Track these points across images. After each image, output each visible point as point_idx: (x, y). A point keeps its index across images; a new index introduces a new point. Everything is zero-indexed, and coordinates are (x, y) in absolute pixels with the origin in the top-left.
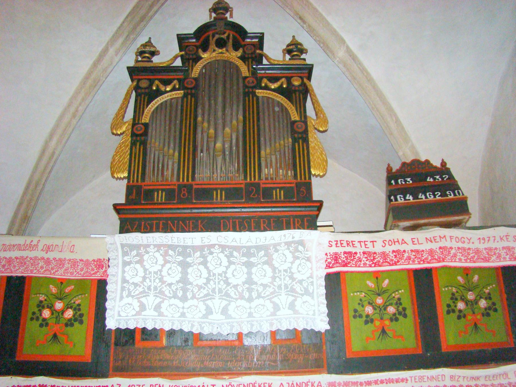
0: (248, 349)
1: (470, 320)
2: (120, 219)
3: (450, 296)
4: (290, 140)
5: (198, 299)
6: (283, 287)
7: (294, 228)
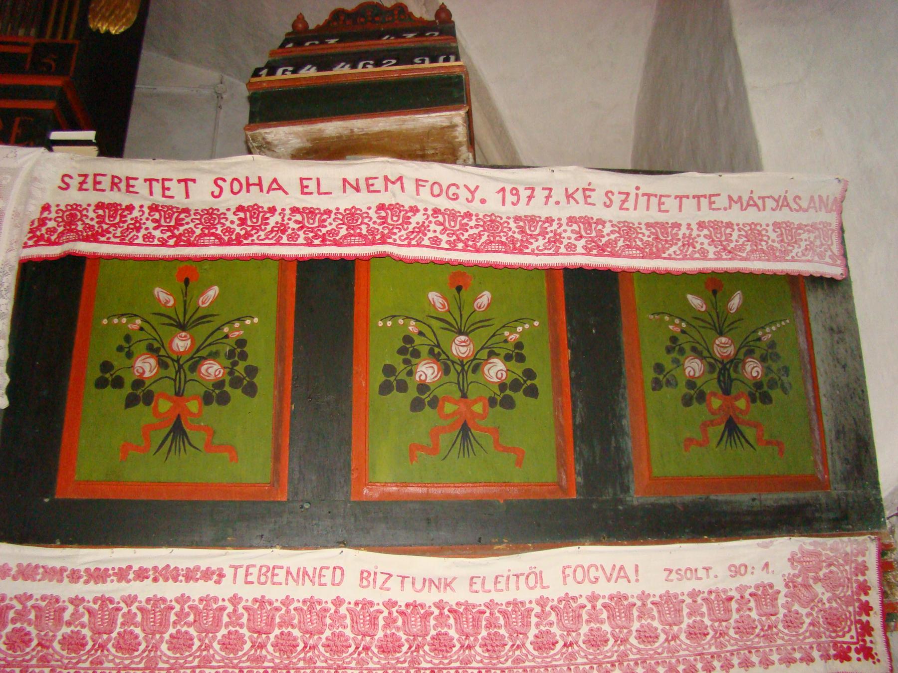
1: (448, 416)
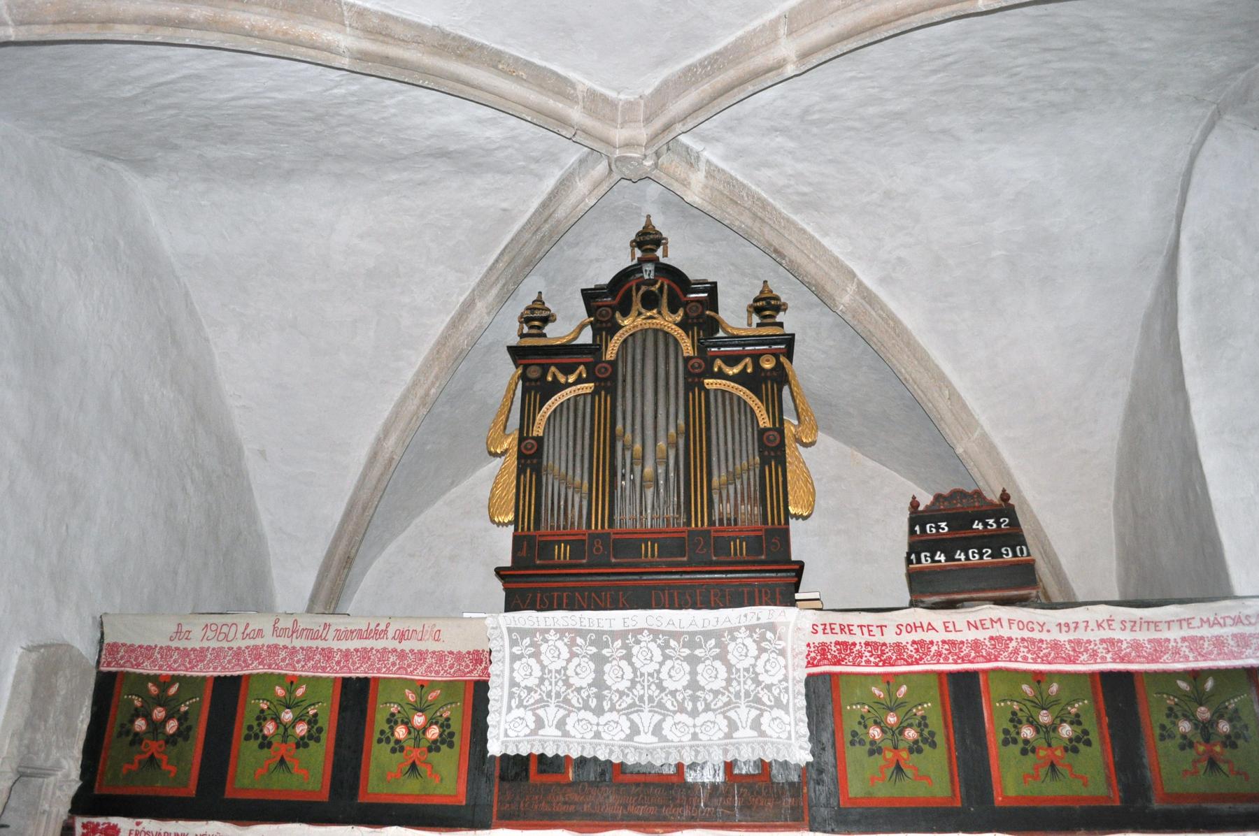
0: (692, 787)
2: (506, 589)
3: (1010, 716)
4: (757, 458)
5: (618, 711)
6: (742, 694)
7: (761, 604)
